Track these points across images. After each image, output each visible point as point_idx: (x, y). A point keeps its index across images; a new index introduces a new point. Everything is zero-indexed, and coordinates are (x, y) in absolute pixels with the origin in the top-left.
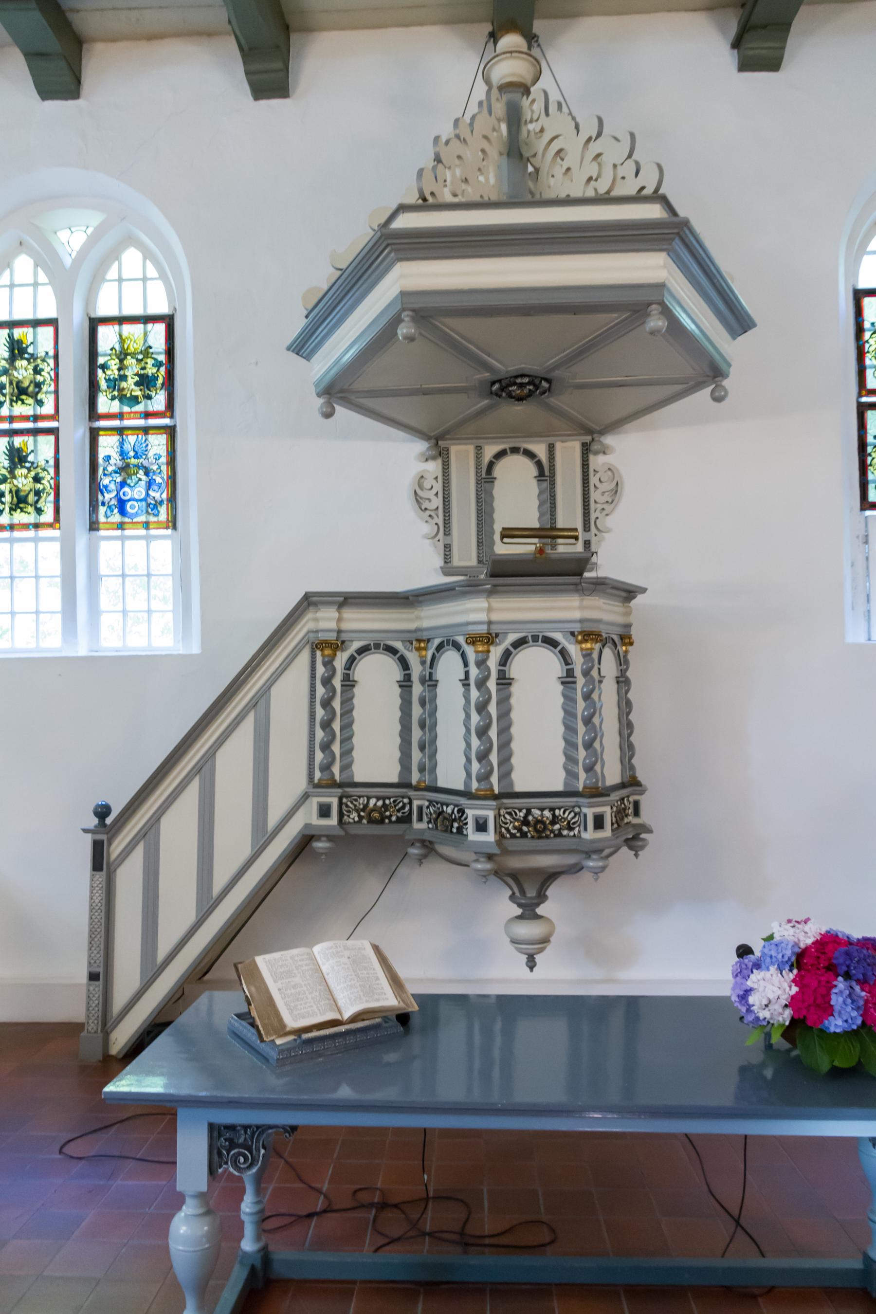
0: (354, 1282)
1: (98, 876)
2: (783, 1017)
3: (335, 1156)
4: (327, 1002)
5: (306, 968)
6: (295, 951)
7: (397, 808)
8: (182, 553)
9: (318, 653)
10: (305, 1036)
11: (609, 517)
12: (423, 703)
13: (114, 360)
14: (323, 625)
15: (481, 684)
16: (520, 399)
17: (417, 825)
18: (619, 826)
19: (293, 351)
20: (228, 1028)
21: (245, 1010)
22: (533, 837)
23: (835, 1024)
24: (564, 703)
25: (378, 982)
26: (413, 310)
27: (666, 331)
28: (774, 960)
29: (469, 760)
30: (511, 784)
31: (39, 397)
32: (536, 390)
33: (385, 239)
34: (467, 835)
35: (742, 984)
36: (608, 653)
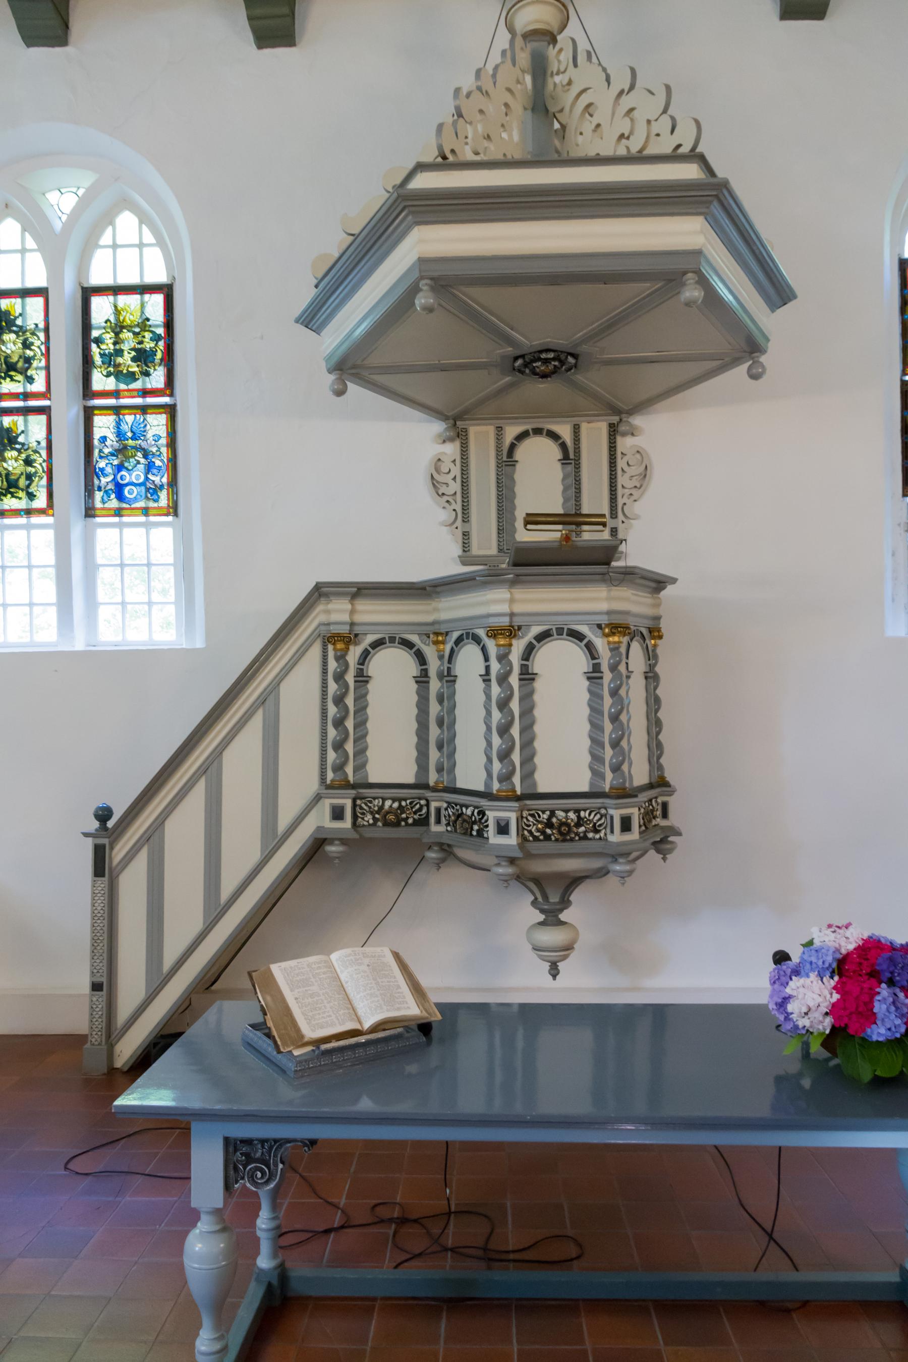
0: (374, 1299)
1: (100, 882)
2: (823, 1025)
3: (352, 1170)
4: (346, 1011)
5: (324, 976)
6: (304, 962)
7: (414, 810)
8: (184, 543)
9: (330, 647)
10: (324, 1047)
11: (637, 502)
12: (440, 700)
13: (109, 333)
14: (335, 617)
15: (503, 679)
16: (544, 376)
17: (434, 828)
18: (646, 828)
19: (302, 324)
20: (242, 1039)
21: (261, 1020)
22: (557, 840)
23: (878, 1032)
24: (590, 700)
25: (399, 990)
26: (432, 279)
27: (702, 302)
28: (814, 966)
29: (490, 760)
30: (535, 784)
31: (29, 373)
32: (562, 366)
33: (403, 200)
34: (488, 838)
35: (780, 991)
36: (636, 646)
